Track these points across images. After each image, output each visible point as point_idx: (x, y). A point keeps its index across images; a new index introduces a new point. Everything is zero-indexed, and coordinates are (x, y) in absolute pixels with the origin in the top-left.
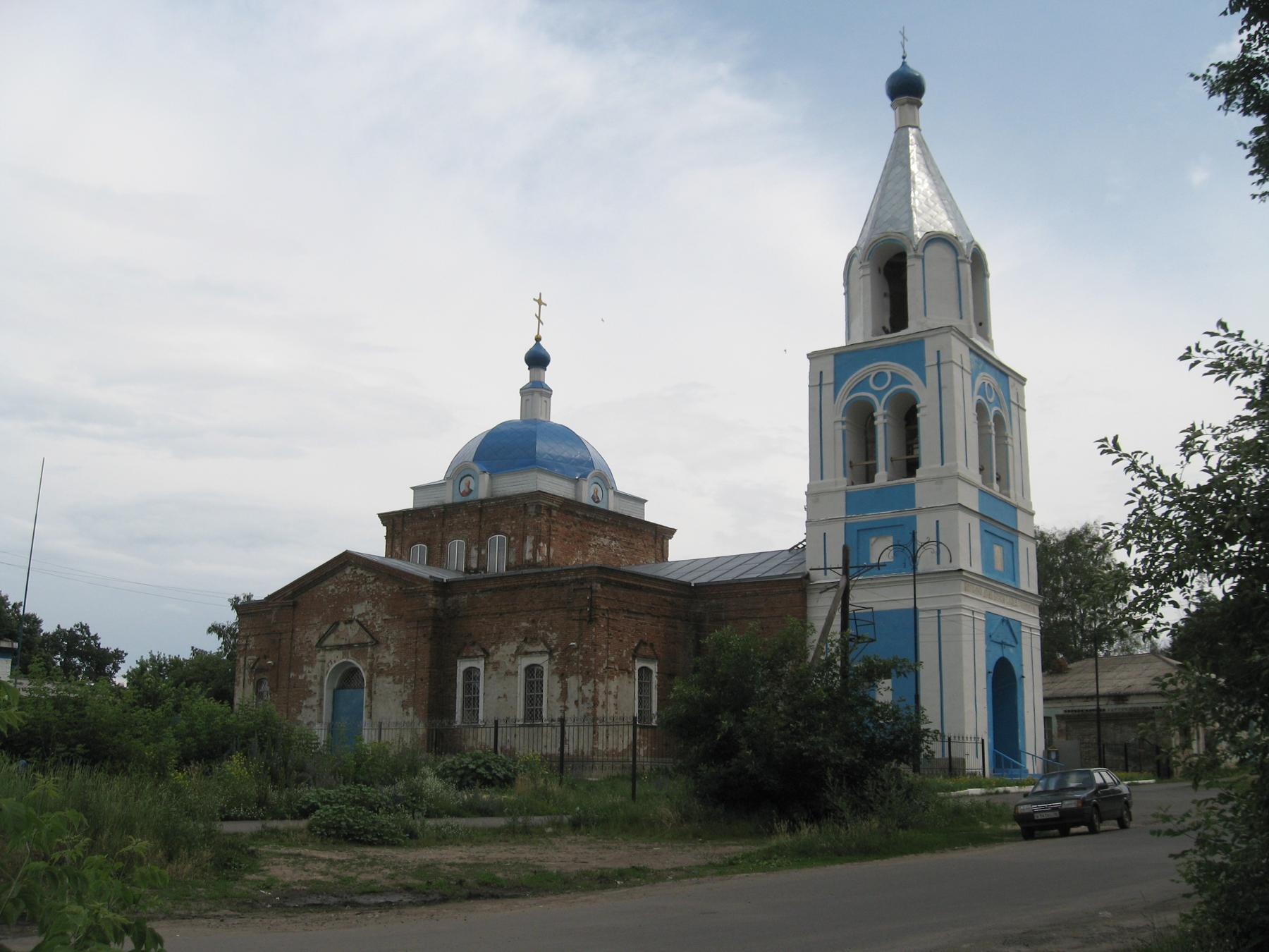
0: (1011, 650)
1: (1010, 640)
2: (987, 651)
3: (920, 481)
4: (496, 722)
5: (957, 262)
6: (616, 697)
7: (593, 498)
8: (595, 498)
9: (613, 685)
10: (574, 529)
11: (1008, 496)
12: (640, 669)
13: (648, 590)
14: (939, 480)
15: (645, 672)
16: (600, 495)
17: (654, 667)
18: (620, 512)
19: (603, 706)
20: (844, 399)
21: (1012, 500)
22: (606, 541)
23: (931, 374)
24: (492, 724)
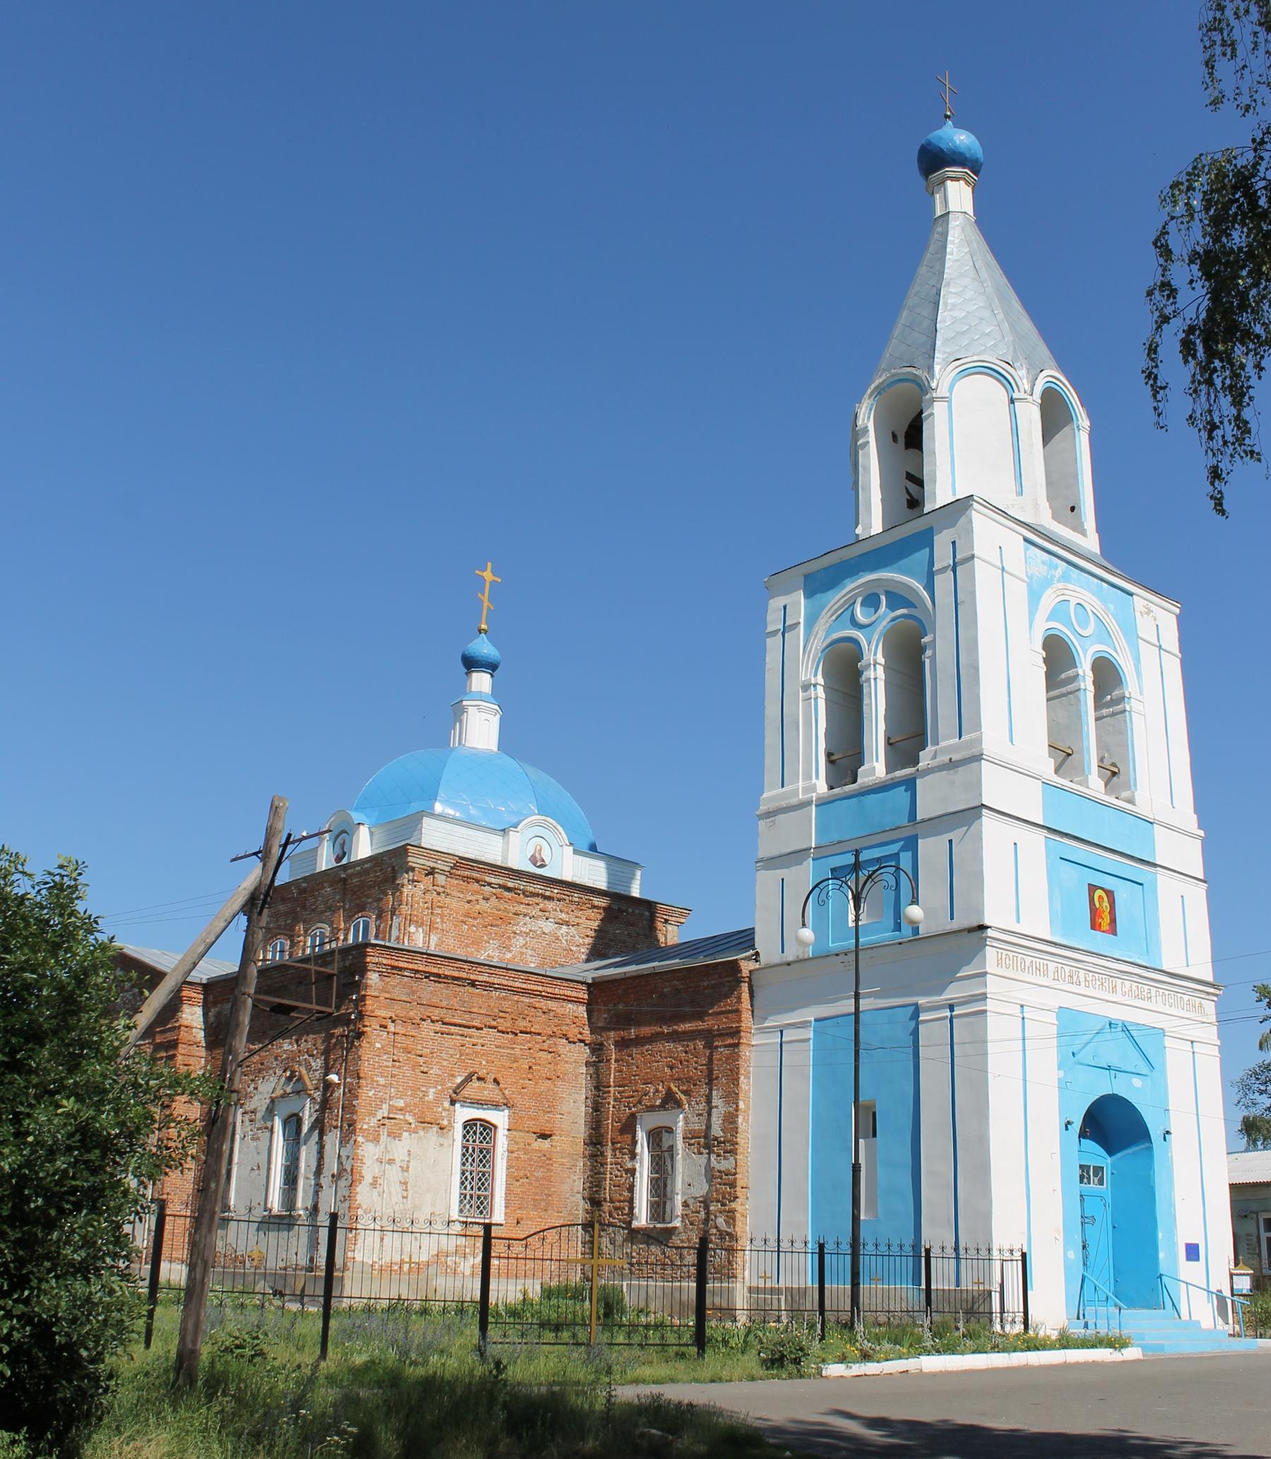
0: (1137, 1082)
1: (1144, 1069)
2: (1063, 1085)
3: (929, 771)
4: (821, 1247)
5: (1012, 401)
6: (405, 1169)
7: (533, 860)
8: (536, 861)
9: (399, 1149)
10: (484, 905)
11: (1131, 801)
12: (469, 1125)
13: (488, 986)
14: (952, 765)
15: (479, 1131)
16: (546, 855)
17: (500, 1118)
18: (578, 882)
19: (374, 1184)
20: (819, 641)
21: (1142, 808)
22: (549, 926)
23: (943, 583)
24: (1018, 1255)
